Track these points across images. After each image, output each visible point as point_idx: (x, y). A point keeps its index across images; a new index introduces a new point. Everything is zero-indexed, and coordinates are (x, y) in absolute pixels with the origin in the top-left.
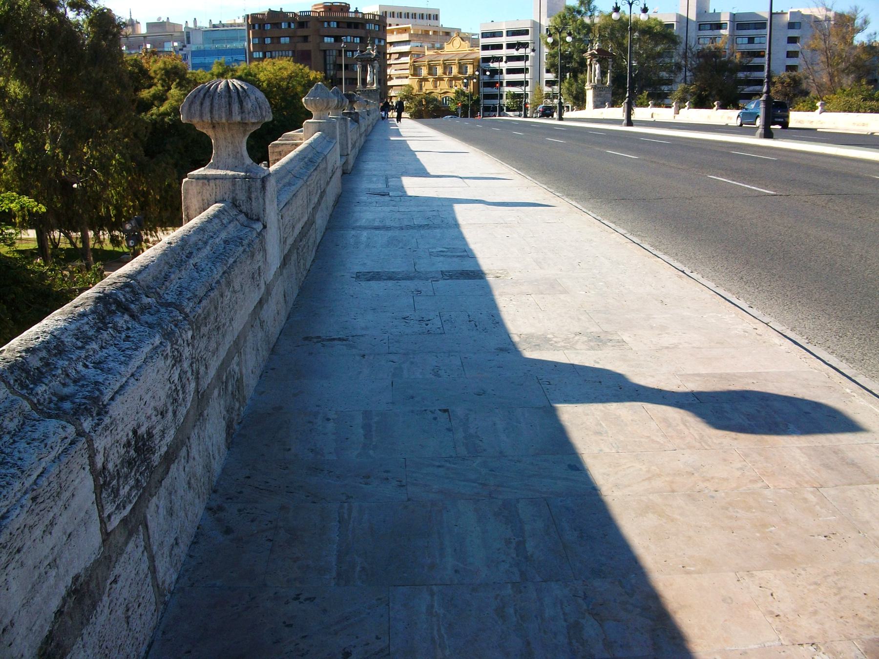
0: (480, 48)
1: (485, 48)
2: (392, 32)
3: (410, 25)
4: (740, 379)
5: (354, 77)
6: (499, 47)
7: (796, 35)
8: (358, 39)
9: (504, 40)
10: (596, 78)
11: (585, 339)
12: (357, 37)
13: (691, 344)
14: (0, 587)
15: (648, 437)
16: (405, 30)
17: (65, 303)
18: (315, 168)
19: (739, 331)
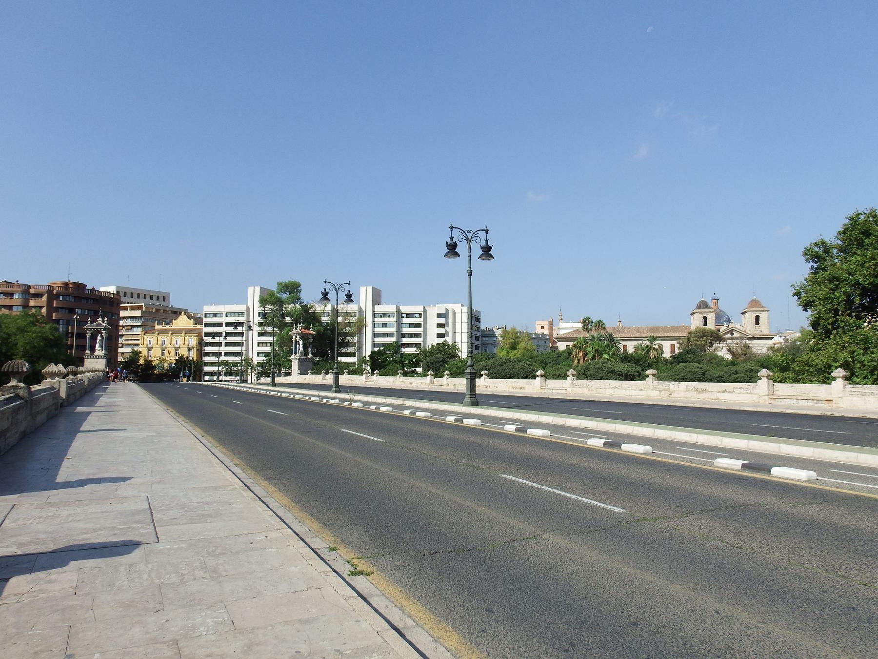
0: (203, 325)
1: (207, 325)
5: (83, 344)
6: (220, 325)
7: (449, 326)
8: (92, 312)
10: (300, 351)
12: (91, 310)
14: (470, 658)
16: (139, 308)
17: (631, 442)
18: (635, 389)
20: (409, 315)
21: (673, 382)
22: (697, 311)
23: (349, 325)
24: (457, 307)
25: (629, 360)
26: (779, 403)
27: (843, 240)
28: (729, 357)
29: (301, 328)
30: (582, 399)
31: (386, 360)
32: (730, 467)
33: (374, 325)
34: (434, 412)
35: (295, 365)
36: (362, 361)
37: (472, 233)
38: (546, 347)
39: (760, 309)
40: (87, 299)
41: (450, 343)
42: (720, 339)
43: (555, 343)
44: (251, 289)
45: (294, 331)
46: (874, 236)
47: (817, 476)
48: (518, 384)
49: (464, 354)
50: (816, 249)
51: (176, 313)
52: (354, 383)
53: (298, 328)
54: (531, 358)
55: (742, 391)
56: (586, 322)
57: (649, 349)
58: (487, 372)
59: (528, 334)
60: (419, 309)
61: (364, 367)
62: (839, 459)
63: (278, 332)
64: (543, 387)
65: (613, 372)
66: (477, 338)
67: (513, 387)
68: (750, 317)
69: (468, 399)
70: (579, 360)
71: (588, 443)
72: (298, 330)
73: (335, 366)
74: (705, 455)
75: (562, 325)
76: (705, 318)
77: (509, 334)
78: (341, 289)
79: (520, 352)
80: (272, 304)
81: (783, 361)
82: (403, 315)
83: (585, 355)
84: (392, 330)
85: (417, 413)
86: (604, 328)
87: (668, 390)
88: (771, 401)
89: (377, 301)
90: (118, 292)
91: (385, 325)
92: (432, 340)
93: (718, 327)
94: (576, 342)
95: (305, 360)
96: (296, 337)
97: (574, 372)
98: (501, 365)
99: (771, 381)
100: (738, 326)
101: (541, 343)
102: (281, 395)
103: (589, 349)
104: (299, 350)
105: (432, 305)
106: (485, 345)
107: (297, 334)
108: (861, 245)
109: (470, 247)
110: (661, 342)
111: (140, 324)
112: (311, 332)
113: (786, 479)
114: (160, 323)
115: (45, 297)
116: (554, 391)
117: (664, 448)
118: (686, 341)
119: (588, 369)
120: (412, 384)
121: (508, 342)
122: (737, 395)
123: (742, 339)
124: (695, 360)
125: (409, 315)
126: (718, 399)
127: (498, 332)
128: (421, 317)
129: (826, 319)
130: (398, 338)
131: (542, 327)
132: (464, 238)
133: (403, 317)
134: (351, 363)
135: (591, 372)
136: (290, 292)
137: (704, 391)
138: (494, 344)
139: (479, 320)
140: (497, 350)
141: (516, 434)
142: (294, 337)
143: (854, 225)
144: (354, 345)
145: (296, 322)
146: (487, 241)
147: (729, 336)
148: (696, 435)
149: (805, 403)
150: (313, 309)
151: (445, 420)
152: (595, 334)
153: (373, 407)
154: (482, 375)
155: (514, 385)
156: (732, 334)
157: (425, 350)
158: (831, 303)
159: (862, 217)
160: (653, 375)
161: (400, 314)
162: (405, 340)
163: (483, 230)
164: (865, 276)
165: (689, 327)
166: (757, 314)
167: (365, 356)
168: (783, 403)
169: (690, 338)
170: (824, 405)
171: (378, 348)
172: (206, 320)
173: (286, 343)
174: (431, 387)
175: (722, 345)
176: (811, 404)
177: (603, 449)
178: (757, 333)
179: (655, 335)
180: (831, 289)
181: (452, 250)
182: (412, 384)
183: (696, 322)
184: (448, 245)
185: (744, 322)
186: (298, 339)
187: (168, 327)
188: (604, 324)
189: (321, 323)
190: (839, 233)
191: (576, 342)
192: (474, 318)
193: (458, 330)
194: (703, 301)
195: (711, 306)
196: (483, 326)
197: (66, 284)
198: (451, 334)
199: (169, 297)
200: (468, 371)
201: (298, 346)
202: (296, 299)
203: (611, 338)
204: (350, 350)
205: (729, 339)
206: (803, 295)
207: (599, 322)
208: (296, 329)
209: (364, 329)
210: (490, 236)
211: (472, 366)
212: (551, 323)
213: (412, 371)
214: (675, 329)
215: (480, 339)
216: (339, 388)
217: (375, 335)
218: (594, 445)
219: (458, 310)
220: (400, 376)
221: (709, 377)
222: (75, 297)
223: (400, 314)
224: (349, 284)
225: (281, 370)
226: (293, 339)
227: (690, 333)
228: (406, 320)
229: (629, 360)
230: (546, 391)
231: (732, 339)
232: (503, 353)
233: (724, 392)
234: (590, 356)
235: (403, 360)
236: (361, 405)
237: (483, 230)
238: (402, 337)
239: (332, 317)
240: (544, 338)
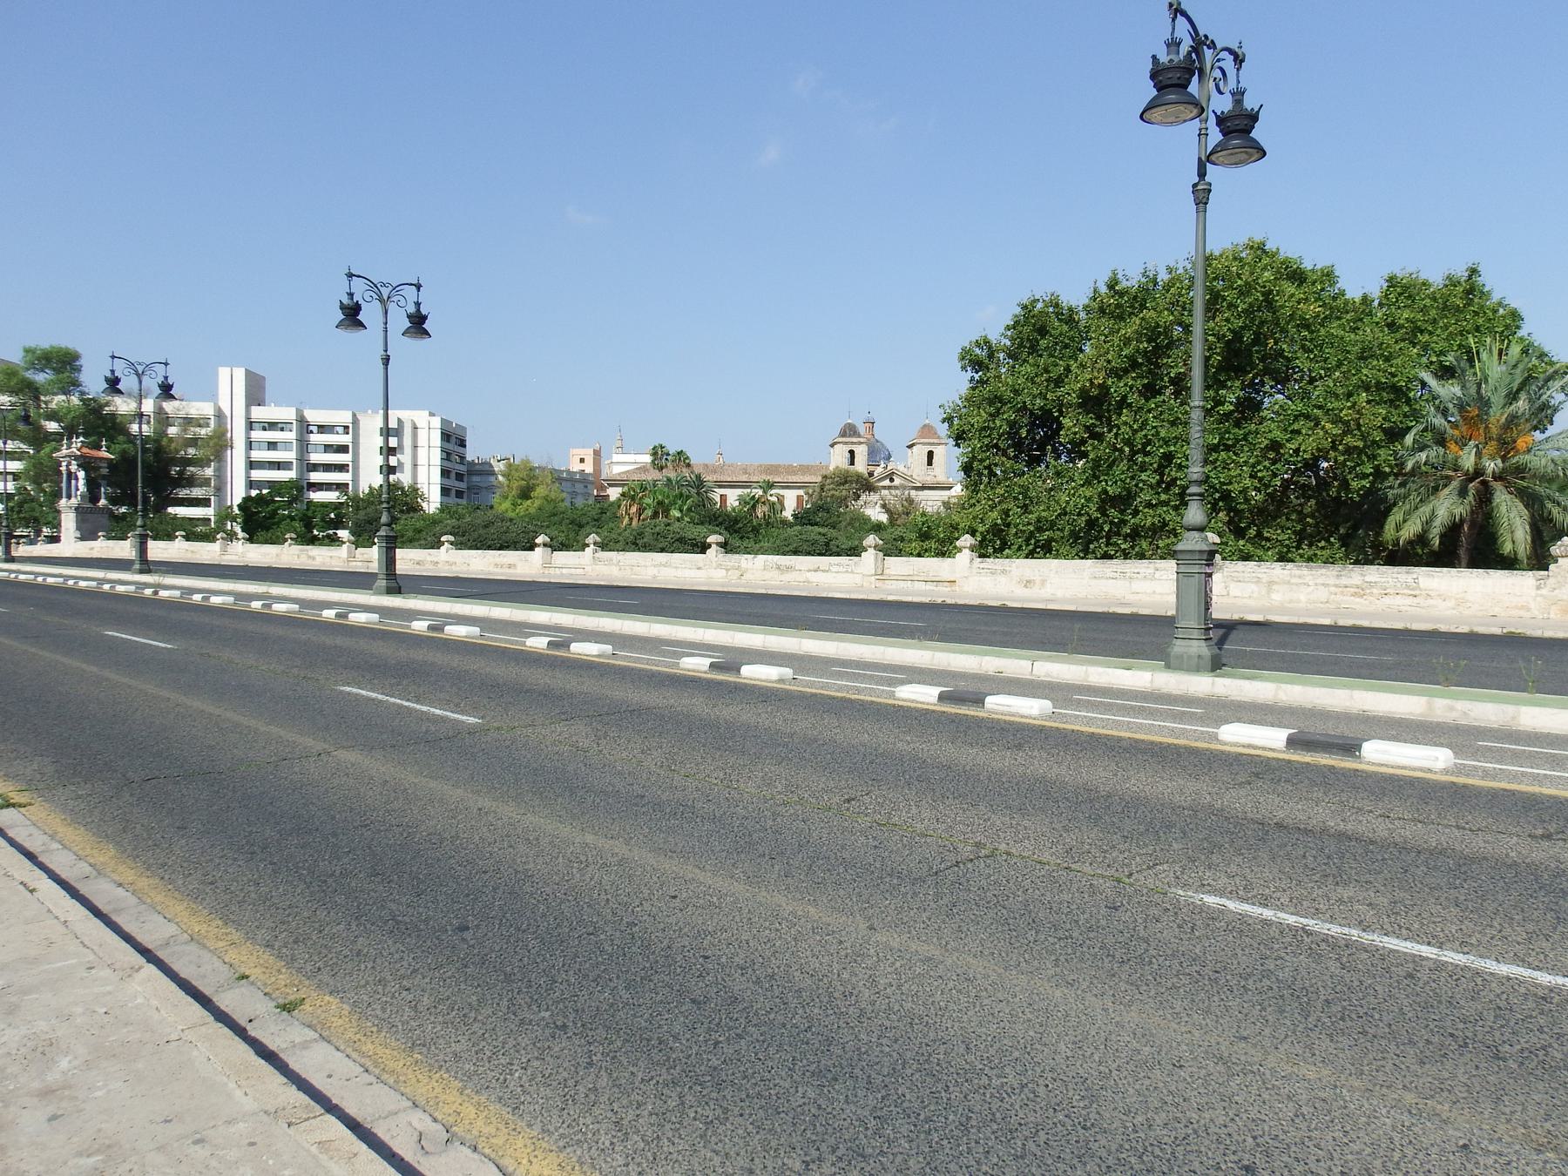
20: (323, 429)
21: (746, 556)
22: (840, 440)
23: (194, 442)
24: (421, 417)
25: (720, 519)
26: (889, 587)
27: (1012, 339)
28: (884, 518)
29: (79, 445)
30: (602, 583)
31: (274, 512)
32: (696, 668)
33: (250, 445)
34: (303, 603)
35: (69, 521)
36: (225, 515)
37: (390, 288)
38: (587, 495)
39: (936, 441)
41: (405, 485)
42: (870, 488)
43: (603, 488)
44: (224, 373)
45: (64, 451)
46: (1051, 336)
47: (1054, 708)
48: (505, 560)
49: (432, 501)
50: (978, 351)
52: (198, 556)
53: (74, 445)
54: (555, 515)
55: (841, 569)
56: (658, 453)
57: (754, 502)
58: (451, 538)
59: (553, 471)
60: (345, 417)
61: (229, 528)
62: (587, 625)
63: (31, 452)
64: (547, 564)
65: (681, 540)
66: (459, 477)
67: (496, 565)
68: (920, 452)
69: (382, 583)
70: (631, 519)
71: (527, 644)
72: (75, 450)
73: (139, 523)
74: (880, 681)
75: (616, 458)
76: (852, 453)
77: (516, 470)
78: (148, 373)
79: (537, 503)
80: (11, 392)
81: (923, 524)
82: (311, 428)
83: (641, 511)
84: (290, 455)
85: (350, 615)
86: (688, 465)
87: (738, 568)
88: (879, 584)
89: (256, 393)
91: (272, 445)
92: (370, 478)
93: (871, 468)
94: (626, 488)
95: (91, 511)
96: (69, 464)
97: (598, 539)
98: (486, 526)
99: (881, 554)
100: (901, 468)
101: (579, 488)
102: (16, 577)
103: (648, 501)
104: (77, 489)
105: (370, 412)
106: (474, 490)
107: (70, 456)
108: (1034, 349)
109: (386, 313)
110: (781, 492)
112: (104, 454)
113: (1013, 715)
116: (564, 571)
117: (632, 648)
118: (818, 490)
119: (641, 534)
120: (314, 558)
121: (515, 484)
122: (834, 574)
123: (904, 487)
124: (830, 521)
125: (323, 429)
126: (808, 582)
127: (499, 467)
128: (348, 433)
129: (982, 461)
130: (301, 472)
131: (582, 460)
132: (375, 296)
133: (312, 432)
134: (199, 519)
135: (645, 540)
136: (54, 369)
137: (789, 568)
138: (491, 489)
139: (462, 444)
140: (495, 499)
141: (713, 676)
142: (64, 464)
143: (1027, 318)
144: (206, 482)
145: (70, 432)
146: (418, 304)
147: (887, 483)
148: (702, 630)
149: (922, 586)
150: (112, 408)
151: (320, 616)
152: (672, 475)
153: (197, 598)
154: (286, 540)
155: (498, 560)
156: (892, 480)
157: (358, 496)
158: (989, 436)
159: (1040, 305)
160: (718, 544)
161: (304, 427)
162: (316, 477)
163: (412, 284)
164: (1035, 397)
165: (827, 467)
166: (931, 448)
167: (231, 507)
168: (894, 587)
169: (824, 485)
170: (580, 571)
171: (258, 492)
173: (46, 475)
174: (351, 564)
175: (874, 497)
176: (930, 587)
177: (937, 708)
178: (929, 480)
179: (771, 478)
180: (991, 415)
181: (351, 315)
182: (314, 558)
183: (837, 459)
184: (343, 307)
185: (910, 460)
186: (74, 468)
188: (687, 458)
189: (131, 439)
190: (1008, 328)
191: (626, 488)
192: (453, 439)
193: (422, 459)
194: (849, 424)
195: (862, 434)
196: (471, 455)
198: (408, 467)
200: (382, 533)
201: (73, 482)
202: (70, 386)
203: (699, 483)
204: (197, 492)
205: (884, 488)
206: (956, 421)
207: (680, 453)
208: (69, 447)
209: (229, 452)
210: (424, 296)
211: (389, 525)
212: (597, 453)
213: (328, 536)
214: (805, 469)
215: (465, 479)
216: (146, 566)
217: (252, 465)
218: (921, 700)
219: (421, 423)
220: (290, 545)
221: (835, 549)
223: (304, 427)
224: (166, 364)
225: (41, 531)
226: (63, 469)
227: (825, 477)
228: (316, 438)
229: (720, 519)
230: (552, 571)
231: (889, 488)
232: (506, 505)
233: (816, 571)
234: (649, 512)
235: (310, 513)
236: (177, 593)
237: (412, 284)
238: (309, 471)
239: (157, 425)
240: (584, 479)
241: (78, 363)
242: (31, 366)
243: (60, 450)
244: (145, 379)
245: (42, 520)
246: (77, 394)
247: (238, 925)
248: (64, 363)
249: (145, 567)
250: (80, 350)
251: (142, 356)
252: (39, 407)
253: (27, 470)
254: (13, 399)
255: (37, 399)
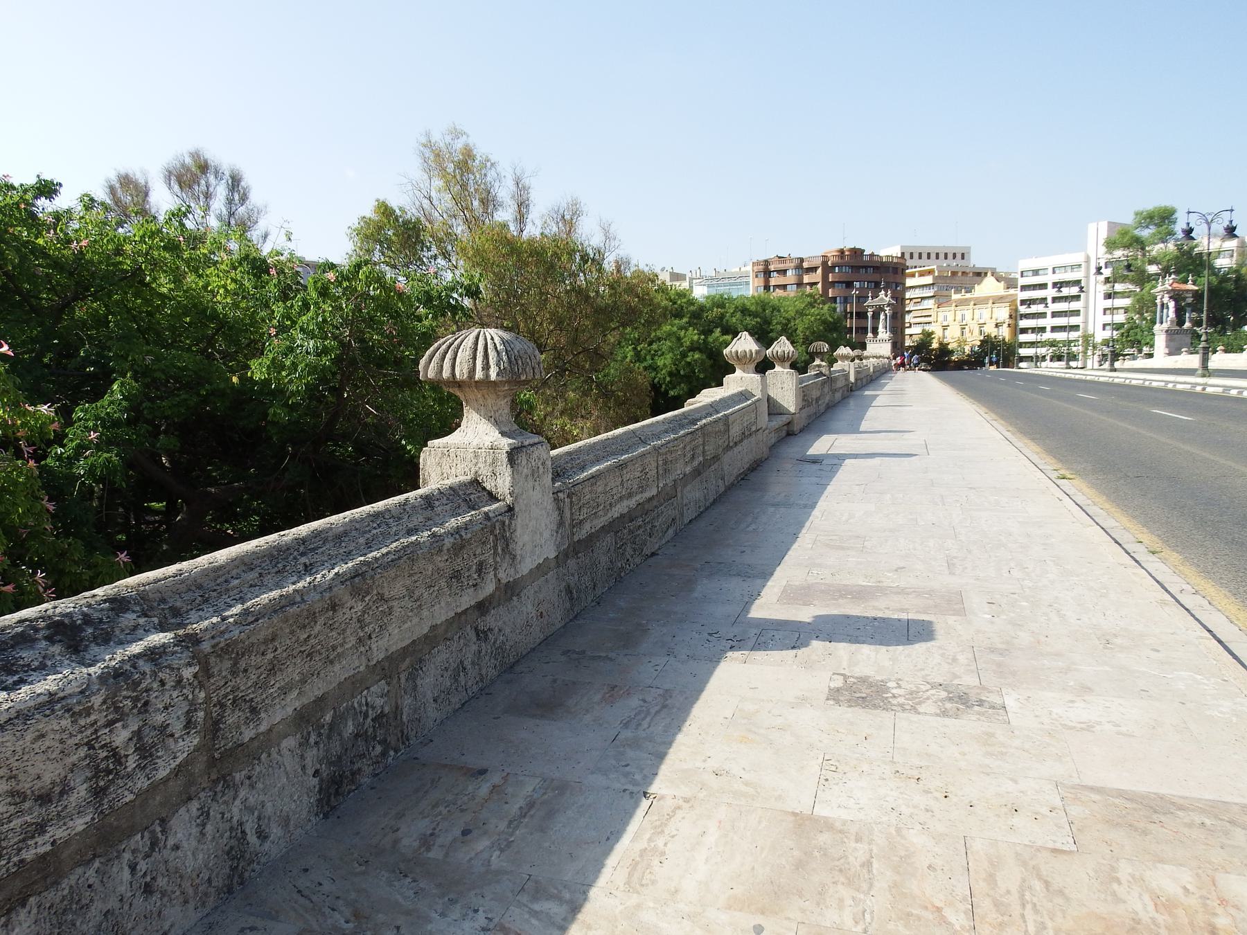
0: (1019, 288)
1: (1024, 288)
2: (913, 275)
3: (935, 267)
4: (1180, 813)
8: (873, 284)
9: (1049, 279)
11: (944, 694)
12: (871, 282)
13: (1118, 726)
15: (939, 910)
16: (930, 272)
19: (1221, 712)
29: (1171, 281)
35: (1160, 341)
40: (866, 267)
45: (1160, 288)
51: (980, 275)
53: (1167, 282)
90: (903, 254)
95: (1177, 332)
96: (1163, 297)
104: (1168, 316)
111: (932, 294)
112: (1190, 286)
114: (958, 291)
115: (819, 271)
136: (1156, 225)
145: (1166, 271)
150: (1200, 249)
172: (1022, 281)
173: (1146, 306)
186: (1166, 300)
187: (968, 295)
197: (842, 252)
199: (969, 253)
201: (1165, 311)
216: (1206, 371)
222: (852, 267)
226: (1158, 301)
241: (1174, 217)
242: (1140, 225)
243: (1156, 287)
244: (1214, 226)
245: (1143, 342)
246: (1172, 242)
247: (1148, 528)
248: (1163, 218)
249: (1206, 372)
250: (1176, 206)
251: (1209, 208)
252: (1144, 255)
253: (1133, 305)
254: (1126, 253)
255: (1143, 249)
